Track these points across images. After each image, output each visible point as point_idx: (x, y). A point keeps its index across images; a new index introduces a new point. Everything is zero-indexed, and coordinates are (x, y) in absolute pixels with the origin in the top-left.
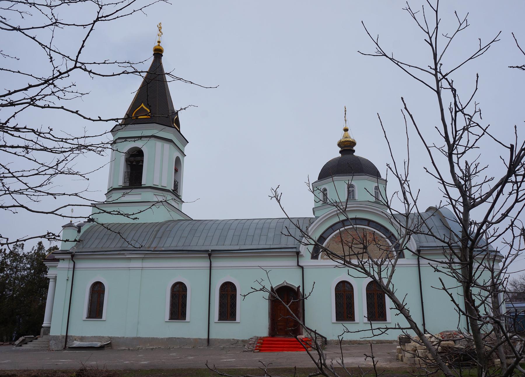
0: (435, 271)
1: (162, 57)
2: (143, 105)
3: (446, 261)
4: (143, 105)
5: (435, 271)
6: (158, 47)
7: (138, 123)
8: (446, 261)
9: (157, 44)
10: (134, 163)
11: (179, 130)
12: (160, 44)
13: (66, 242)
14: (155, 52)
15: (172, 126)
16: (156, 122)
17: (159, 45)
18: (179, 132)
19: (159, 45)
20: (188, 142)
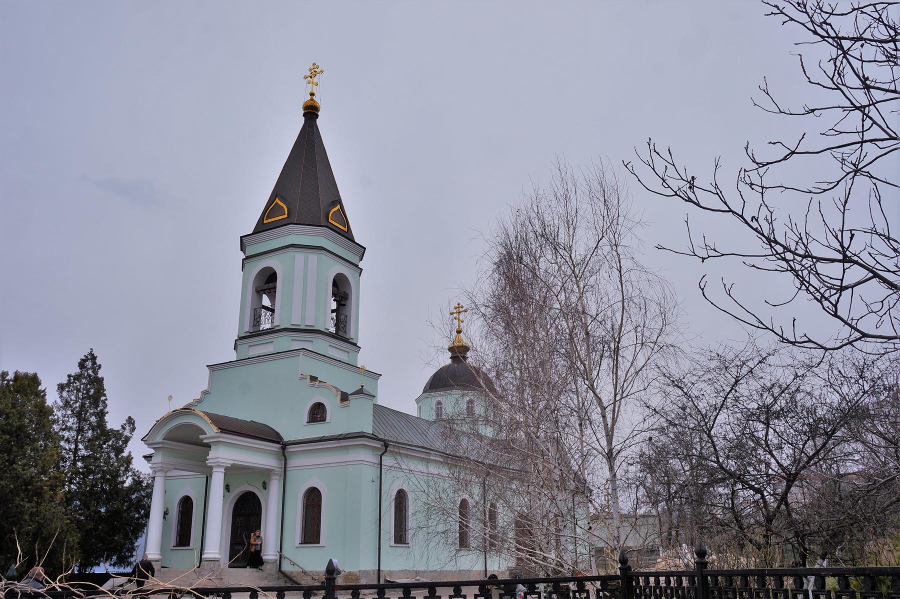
0: (459, 304)
5: (459, 304)
17: (312, 99)
19: (312, 99)
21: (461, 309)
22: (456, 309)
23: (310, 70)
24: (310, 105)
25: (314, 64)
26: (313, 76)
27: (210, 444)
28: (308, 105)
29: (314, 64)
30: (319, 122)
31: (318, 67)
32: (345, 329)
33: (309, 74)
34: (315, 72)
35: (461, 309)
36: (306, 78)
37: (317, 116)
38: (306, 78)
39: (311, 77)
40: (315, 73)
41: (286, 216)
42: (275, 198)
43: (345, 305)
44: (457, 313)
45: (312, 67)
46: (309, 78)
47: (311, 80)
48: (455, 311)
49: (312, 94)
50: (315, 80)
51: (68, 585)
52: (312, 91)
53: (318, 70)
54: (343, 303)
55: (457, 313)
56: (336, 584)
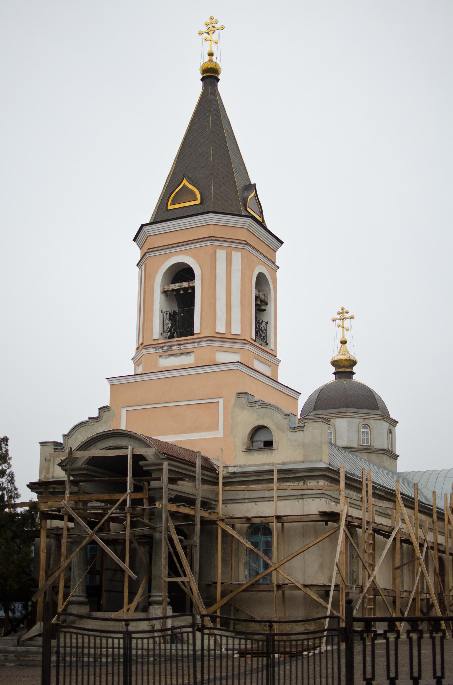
0: (343, 309)
1: (219, 84)
2: (185, 182)
3: (320, 500)
4: (185, 182)
5: (343, 309)
6: (210, 65)
7: (179, 216)
8: (298, 501)
9: (207, 58)
10: (181, 292)
11: (260, 220)
12: (214, 58)
13: (393, 415)
14: (204, 75)
15: (243, 214)
16: (211, 210)
17: (211, 61)
18: (262, 224)
19: (211, 61)
20: (282, 243)
21: (346, 315)
22: (339, 314)
23: (207, 25)
24: (211, 68)
25: (211, 18)
26: (211, 33)
27: (151, 472)
28: (209, 67)
29: (211, 18)
30: (221, 86)
31: (216, 22)
32: (265, 339)
33: (205, 29)
34: (214, 27)
35: (346, 315)
36: (201, 34)
37: (218, 80)
38: (201, 34)
39: (208, 33)
40: (213, 29)
41: (198, 202)
42: (182, 178)
43: (265, 310)
44: (340, 319)
45: (209, 21)
46: (206, 34)
47: (209, 37)
48: (338, 317)
49: (211, 54)
50: (215, 37)
51: (130, 602)
52: (211, 50)
53: (217, 26)
54: (263, 307)
55: (340, 319)
56: (364, 623)
